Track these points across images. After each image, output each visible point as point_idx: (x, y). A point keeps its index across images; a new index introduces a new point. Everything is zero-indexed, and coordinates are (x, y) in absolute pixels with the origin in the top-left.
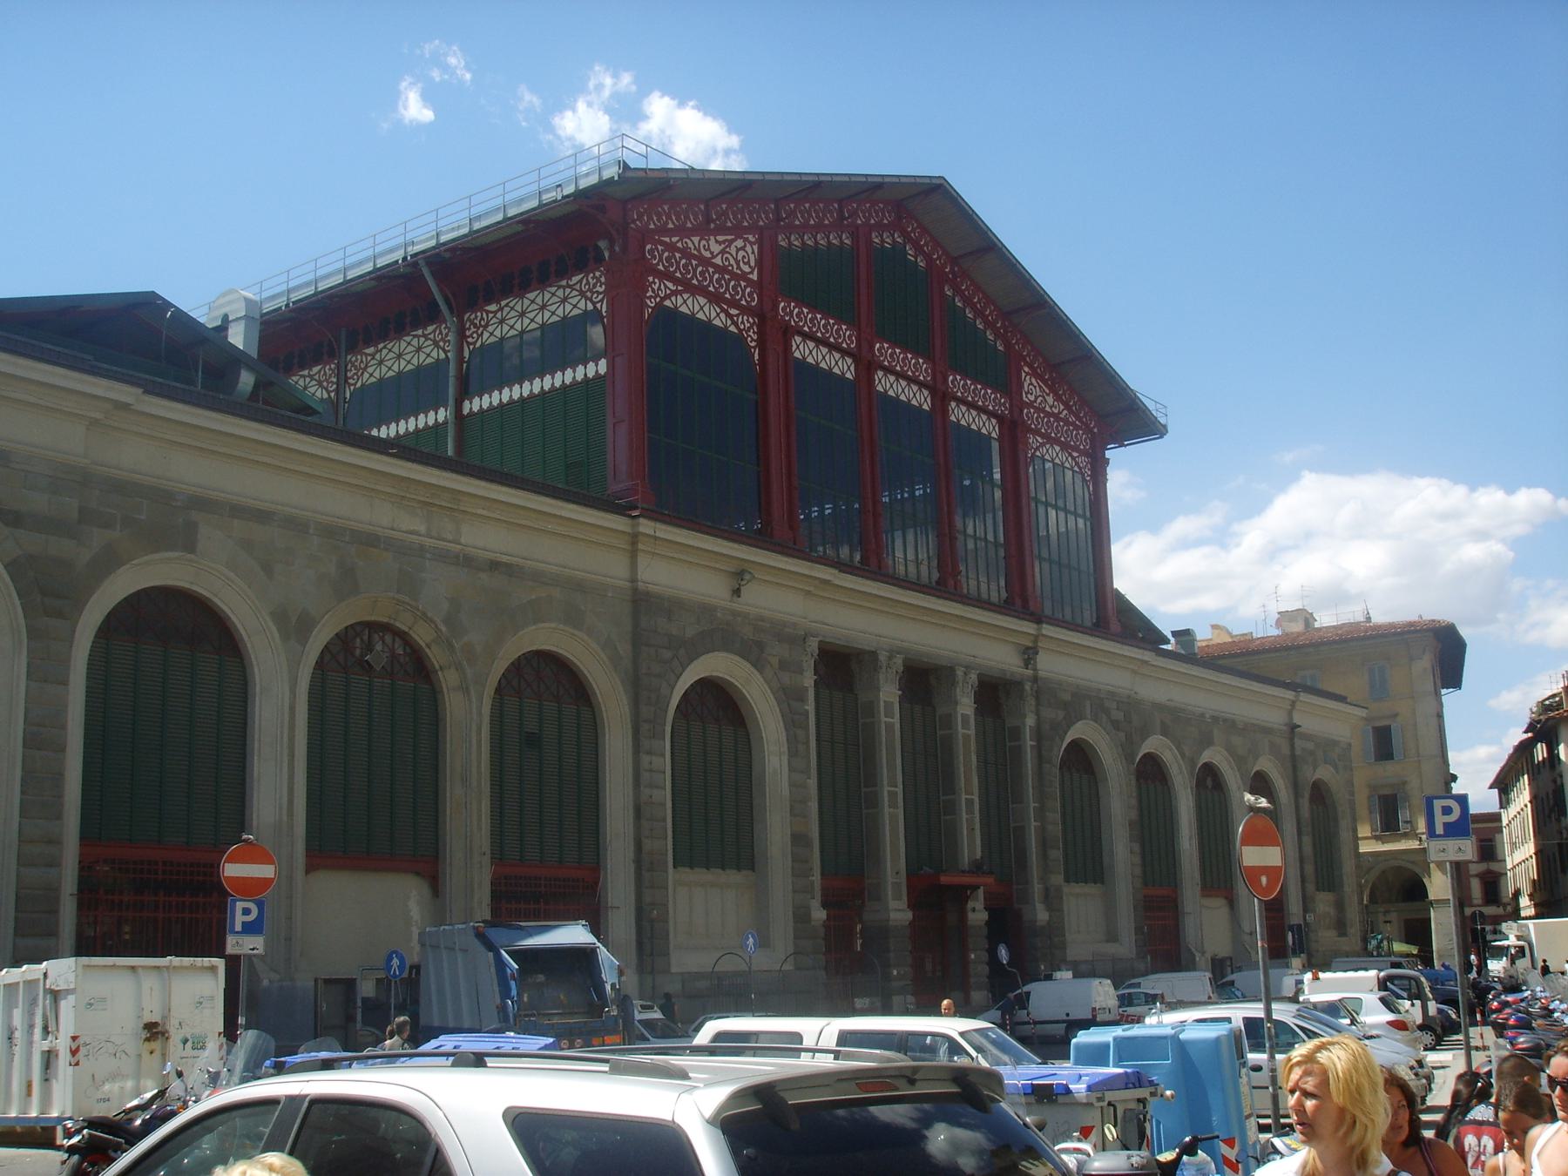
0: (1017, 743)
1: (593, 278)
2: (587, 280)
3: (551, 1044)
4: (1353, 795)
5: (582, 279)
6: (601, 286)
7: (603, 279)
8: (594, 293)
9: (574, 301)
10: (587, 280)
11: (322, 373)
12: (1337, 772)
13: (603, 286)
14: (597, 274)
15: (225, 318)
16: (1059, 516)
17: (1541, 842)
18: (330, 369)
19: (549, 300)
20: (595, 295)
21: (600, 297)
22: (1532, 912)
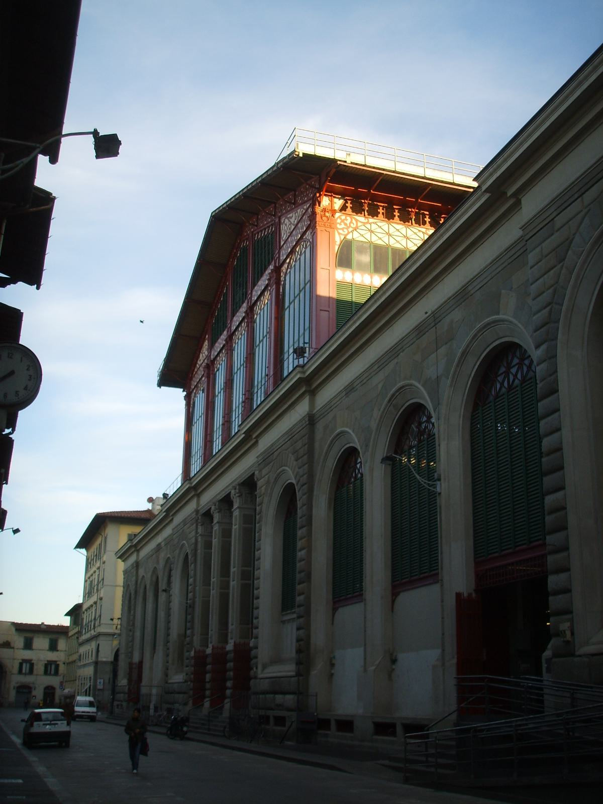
5: (338, 232)
8: (350, 225)
11: (341, 231)
14: (339, 221)
18: (340, 224)
20: (352, 225)
21: (354, 221)
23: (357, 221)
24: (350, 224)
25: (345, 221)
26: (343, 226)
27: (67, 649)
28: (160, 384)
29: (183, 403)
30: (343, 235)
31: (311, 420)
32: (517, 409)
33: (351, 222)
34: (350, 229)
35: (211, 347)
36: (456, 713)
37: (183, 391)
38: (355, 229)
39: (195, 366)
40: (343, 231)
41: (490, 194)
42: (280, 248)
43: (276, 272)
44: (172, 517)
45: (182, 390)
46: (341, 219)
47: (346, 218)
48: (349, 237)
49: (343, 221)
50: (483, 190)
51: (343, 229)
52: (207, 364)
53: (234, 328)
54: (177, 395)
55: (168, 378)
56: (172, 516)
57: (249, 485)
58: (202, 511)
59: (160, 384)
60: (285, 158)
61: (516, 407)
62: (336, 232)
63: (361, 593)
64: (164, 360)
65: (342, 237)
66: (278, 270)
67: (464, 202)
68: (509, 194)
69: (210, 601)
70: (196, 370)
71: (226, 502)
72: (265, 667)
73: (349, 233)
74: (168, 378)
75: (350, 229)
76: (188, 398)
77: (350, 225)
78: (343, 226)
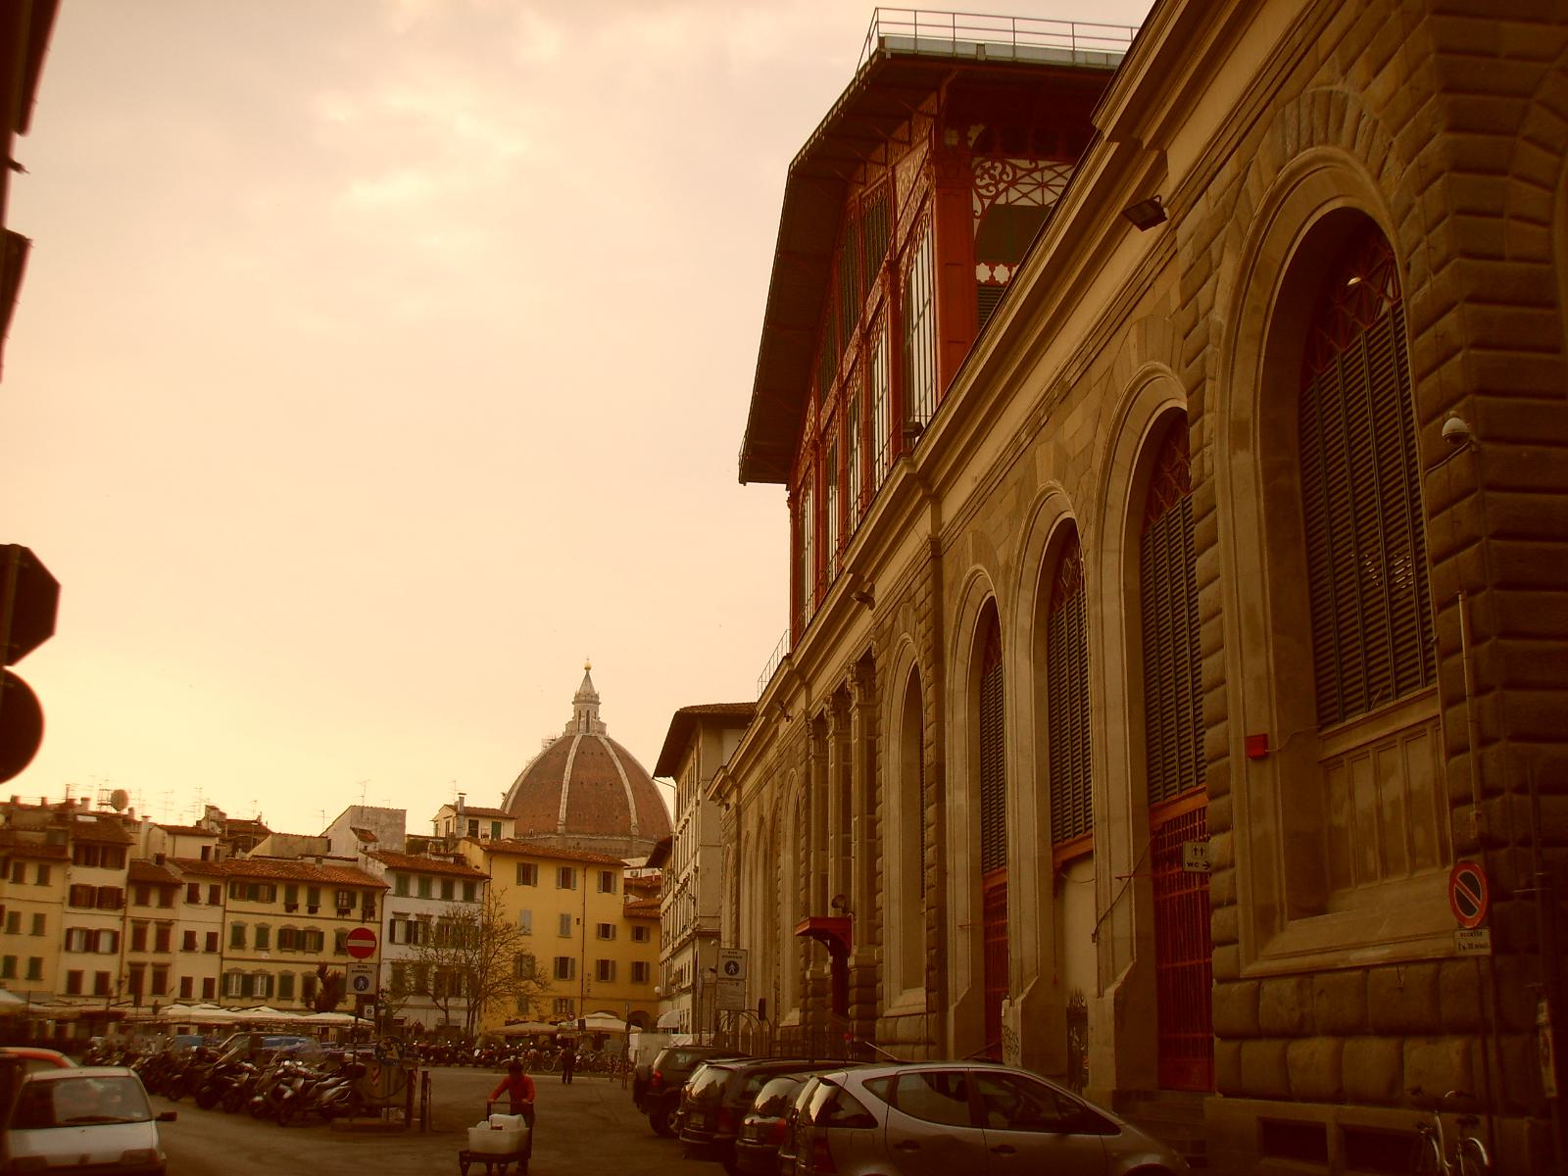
0: (1000, 939)
1: (982, 179)
2: (982, 187)
3: (628, 1056)
4: (1228, 905)
5: (978, 194)
6: (995, 169)
7: (988, 164)
8: (1001, 178)
9: (1025, 189)
10: (982, 187)
12: (1214, 484)
13: (996, 165)
14: (979, 172)
15: (197, 822)
16: (313, 966)
17: (140, 839)
19: (1068, 170)
20: (1005, 177)
21: (1008, 169)
22: (461, 898)
23: (1014, 168)
24: (1001, 174)
25: (992, 172)
26: (987, 180)
27: (451, 1024)
28: (743, 480)
29: (785, 513)
30: (988, 197)
31: (936, 549)
32: (1395, 459)
33: (1003, 172)
34: (1002, 186)
35: (819, 407)
36: (886, 1082)
37: (787, 490)
38: (1013, 183)
39: (800, 446)
40: (988, 190)
41: (1118, 144)
42: (897, 224)
43: (891, 273)
44: (776, 725)
45: (785, 486)
46: (983, 168)
47: (993, 164)
48: (1001, 200)
49: (986, 171)
50: (1105, 138)
51: (986, 187)
52: (815, 442)
53: (845, 375)
54: (776, 495)
55: (757, 465)
56: (776, 722)
57: (866, 665)
58: (815, 715)
59: (743, 480)
60: (866, 65)
61: (1395, 455)
62: (974, 194)
63: (1088, 832)
64: (745, 436)
65: (987, 202)
66: (894, 267)
67: (1087, 154)
68: (1145, 144)
69: (827, 875)
70: (802, 452)
71: (841, 696)
72: (1266, 922)
73: (998, 194)
74: (757, 465)
75: (1002, 186)
76: (795, 503)
77: (1001, 178)
78: (987, 180)
